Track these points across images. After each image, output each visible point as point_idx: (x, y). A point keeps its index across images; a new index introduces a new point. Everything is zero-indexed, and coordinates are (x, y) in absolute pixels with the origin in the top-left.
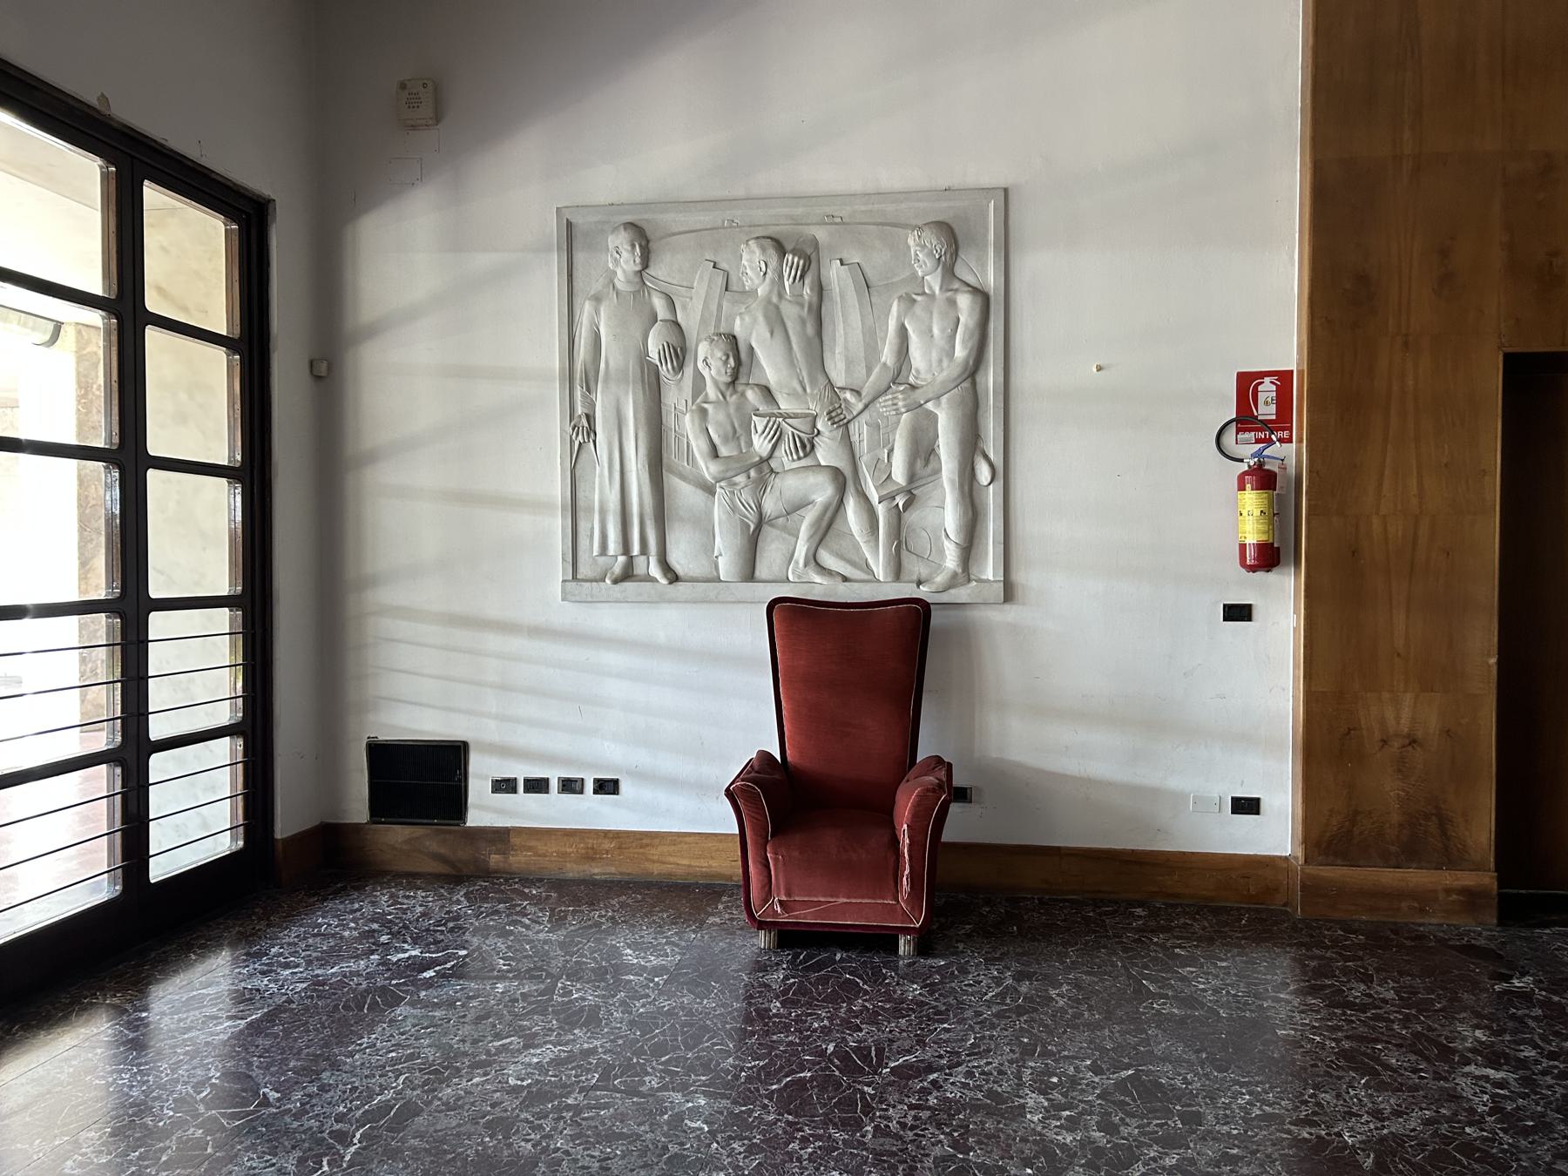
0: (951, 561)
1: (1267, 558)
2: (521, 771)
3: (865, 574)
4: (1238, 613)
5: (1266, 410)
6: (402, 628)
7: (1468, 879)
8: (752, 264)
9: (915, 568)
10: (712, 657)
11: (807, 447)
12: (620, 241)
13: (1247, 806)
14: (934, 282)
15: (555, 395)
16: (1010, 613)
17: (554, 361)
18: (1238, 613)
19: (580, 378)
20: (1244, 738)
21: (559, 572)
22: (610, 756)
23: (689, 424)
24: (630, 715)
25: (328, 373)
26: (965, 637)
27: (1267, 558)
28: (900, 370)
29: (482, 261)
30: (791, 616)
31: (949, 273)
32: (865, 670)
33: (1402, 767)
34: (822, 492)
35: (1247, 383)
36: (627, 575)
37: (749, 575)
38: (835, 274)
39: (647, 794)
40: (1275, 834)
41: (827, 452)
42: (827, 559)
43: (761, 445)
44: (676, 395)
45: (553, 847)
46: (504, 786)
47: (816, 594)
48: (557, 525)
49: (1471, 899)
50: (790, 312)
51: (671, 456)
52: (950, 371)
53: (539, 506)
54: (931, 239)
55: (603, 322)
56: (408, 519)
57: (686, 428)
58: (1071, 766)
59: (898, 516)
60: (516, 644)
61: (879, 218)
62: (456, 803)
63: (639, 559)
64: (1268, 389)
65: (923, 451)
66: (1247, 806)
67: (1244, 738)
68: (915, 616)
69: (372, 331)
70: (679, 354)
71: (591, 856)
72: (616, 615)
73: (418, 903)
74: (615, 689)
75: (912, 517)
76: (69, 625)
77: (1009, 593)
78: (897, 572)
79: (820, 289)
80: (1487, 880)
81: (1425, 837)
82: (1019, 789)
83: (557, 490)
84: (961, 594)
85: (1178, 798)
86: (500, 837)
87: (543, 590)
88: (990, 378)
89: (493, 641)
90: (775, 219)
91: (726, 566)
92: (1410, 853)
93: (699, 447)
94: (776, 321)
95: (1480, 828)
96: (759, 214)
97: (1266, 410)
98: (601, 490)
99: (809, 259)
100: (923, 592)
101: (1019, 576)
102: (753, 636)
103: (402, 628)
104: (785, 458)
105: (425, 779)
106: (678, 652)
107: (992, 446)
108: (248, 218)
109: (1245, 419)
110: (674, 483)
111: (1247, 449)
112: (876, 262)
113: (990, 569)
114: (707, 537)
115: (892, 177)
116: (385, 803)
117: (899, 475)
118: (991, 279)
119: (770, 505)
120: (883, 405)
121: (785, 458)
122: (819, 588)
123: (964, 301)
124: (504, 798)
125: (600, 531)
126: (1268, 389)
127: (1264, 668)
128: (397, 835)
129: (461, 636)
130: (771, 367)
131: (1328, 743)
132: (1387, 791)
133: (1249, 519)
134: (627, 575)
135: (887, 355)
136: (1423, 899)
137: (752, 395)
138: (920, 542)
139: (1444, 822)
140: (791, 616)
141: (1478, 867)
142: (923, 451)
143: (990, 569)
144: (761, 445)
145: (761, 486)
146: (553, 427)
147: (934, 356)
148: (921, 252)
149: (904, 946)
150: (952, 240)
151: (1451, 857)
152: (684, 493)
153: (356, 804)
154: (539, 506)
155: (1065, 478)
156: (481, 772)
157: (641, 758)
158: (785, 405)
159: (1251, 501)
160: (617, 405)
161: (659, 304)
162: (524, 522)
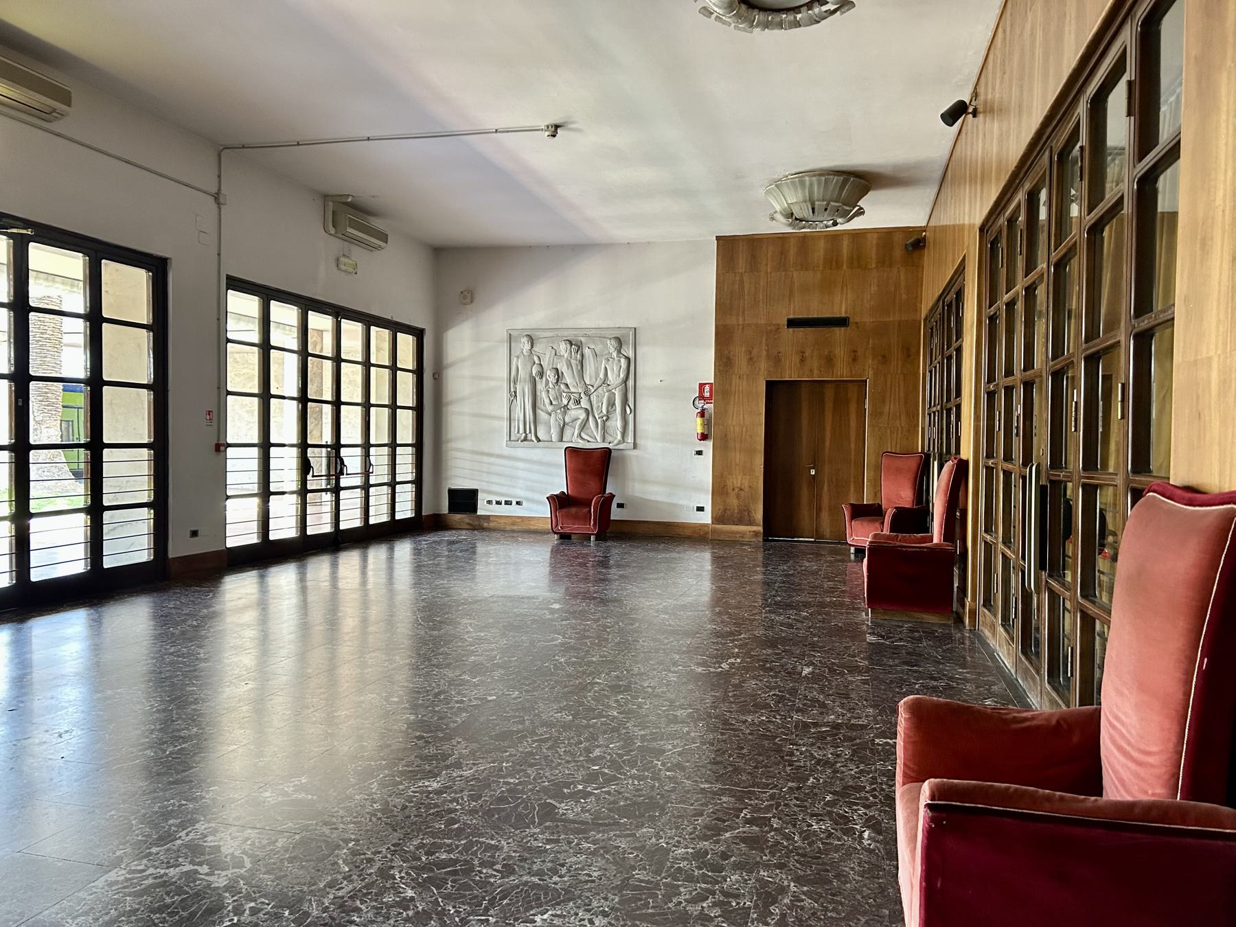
0: (619, 437)
1: (704, 437)
2: (494, 498)
3: (593, 440)
4: (699, 453)
5: (707, 394)
6: (454, 454)
7: (754, 528)
8: (563, 348)
9: (609, 438)
10: (549, 464)
11: (578, 402)
12: (525, 340)
13: (700, 509)
14: (615, 354)
15: (505, 385)
16: (635, 452)
17: (505, 375)
18: (699, 453)
19: (513, 381)
20: (698, 489)
21: (506, 438)
22: (520, 493)
23: (544, 395)
24: (521, 478)
25: (438, 376)
26: (623, 459)
27: (704, 437)
28: (605, 381)
29: (485, 345)
30: (572, 452)
31: (619, 352)
32: (593, 467)
33: (738, 497)
34: (583, 416)
35: (702, 386)
36: (525, 439)
37: (561, 440)
38: (587, 351)
39: (531, 505)
40: (706, 518)
41: (584, 403)
42: (583, 435)
43: (565, 402)
44: (540, 386)
45: (502, 521)
46: (489, 502)
47: (580, 446)
48: (505, 424)
49: (756, 534)
50: (573, 362)
51: (538, 404)
52: (619, 381)
53: (500, 418)
54: (613, 342)
55: (519, 363)
56: (462, 424)
57: (543, 395)
58: (653, 498)
59: (604, 422)
60: (492, 460)
61: (599, 335)
62: (474, 508)
63: (529, 436)
64: (707, 388)
65: (611, 404)
66: (700, 509)
67: (698, 489)
68: (607, 453)
69: (452, 365)
70: (541, 374)
71: (513, 524)
72: (520, 452)
73: (463, 535)
74: (520, 473)
75: (608, 423)
76: (59, 454)
77: (635, 446)
78: (604, 441)
79: (582, 355)
80: (760, 529)
81: (743, 517)
82: (645, 503)
83: (506, 414)
84: (621, 447)
85: (681, 506)
86: (487, 518)
87: (500, 444)
88: (631, 383)
89: (485, 459)
90: (569, 335)
91: (555, 437)
92: (740, 522)
93: (547, 401)
94: (569, 365)
95: (759, 515)
96: (566, 333)
97: (707, 394)
98: (518, 414)
99: (579, 347)
100: (611, 446)
101: (638, 442)
102: (560, 458)
103: (459, 454)
104: (571, 405)
105: (465, 500)
106: (540, 463)
107: (631, 403)
108: (419, 334)
109: (701, 397)
110: (538, 411)
111: (700, 404)
112: (598, 349)
113: (630, 439)
114: (548, 428)
115: (603, 324)
116: (454, 508)
117: (604, 412)
118: (631, 354)
119: (567, 420)
120: (600, 390)
121: (571, 405)
122: (581, 444)
123: (623, 360)
124: (490, 506)
125: (518, 425)
126: (707, 388)
127: (703, 470)
128: (457, 517)
129: (477, 457)
130: (568, 379)
131: (720, 489)
132: (734, 502)
133: (698, 426)
134: (525, 439)
135: (602, 376)
136: (743, 534)
137: (563, 387)
138: (611, 431)
139: (749, 512)
140: (572, 452)
141: (758, 525)
142: (611, 404)
143: (630, 439)
144: (565, 402)
145: (565, 413)
146: (504, 396)
147: (615, 378)
148: (611, 346)
149: (592, 538)
150: (620, 342)
151: (751, 523)
152: (542, 415)
153: (445, 509)
154: (500, 418)
155: (650, 412)
156: (482, 499)
157: (530, 495)
158: (572, 390)
159: (699, 420)
160: (524, 388)
161: (536, 359)
162: (496, 423)
